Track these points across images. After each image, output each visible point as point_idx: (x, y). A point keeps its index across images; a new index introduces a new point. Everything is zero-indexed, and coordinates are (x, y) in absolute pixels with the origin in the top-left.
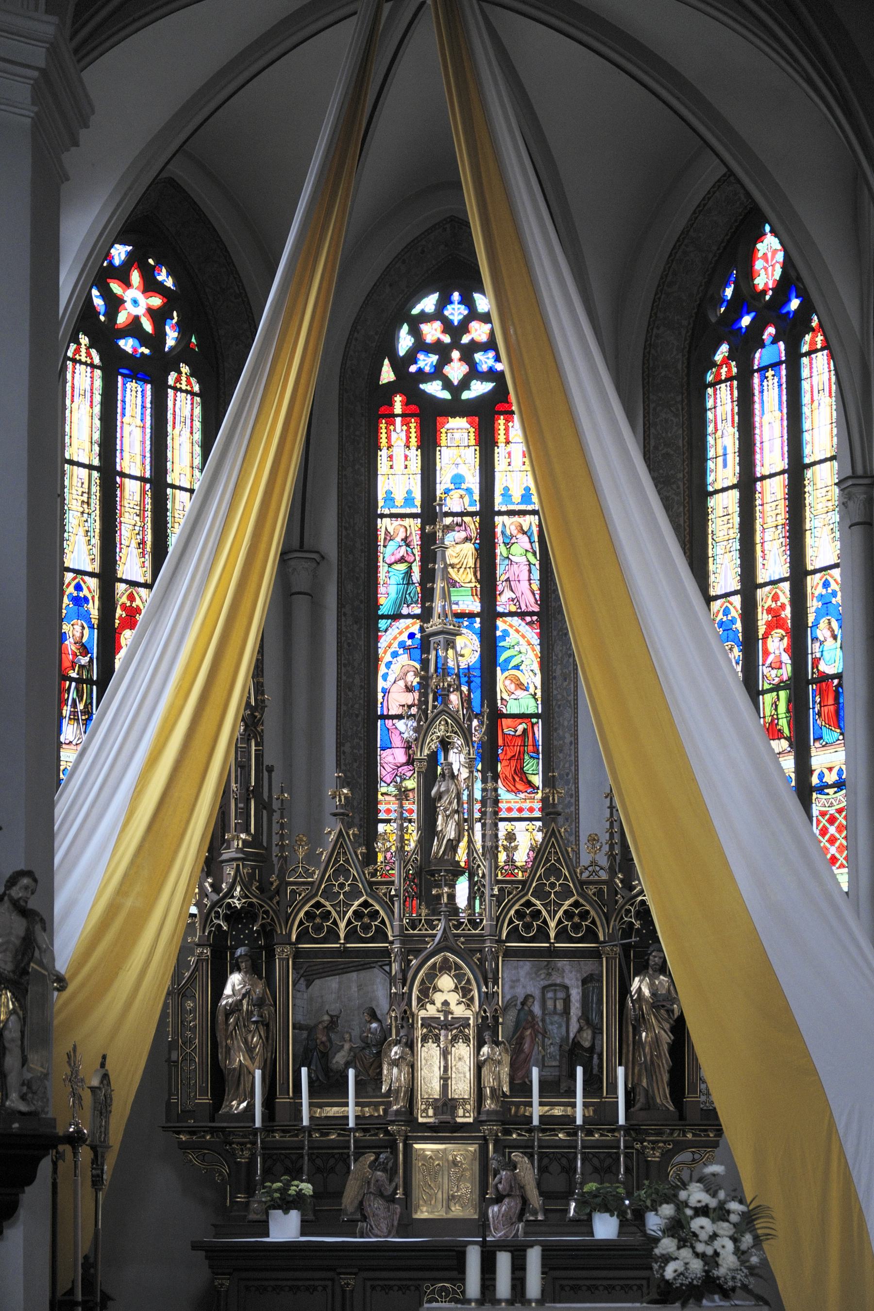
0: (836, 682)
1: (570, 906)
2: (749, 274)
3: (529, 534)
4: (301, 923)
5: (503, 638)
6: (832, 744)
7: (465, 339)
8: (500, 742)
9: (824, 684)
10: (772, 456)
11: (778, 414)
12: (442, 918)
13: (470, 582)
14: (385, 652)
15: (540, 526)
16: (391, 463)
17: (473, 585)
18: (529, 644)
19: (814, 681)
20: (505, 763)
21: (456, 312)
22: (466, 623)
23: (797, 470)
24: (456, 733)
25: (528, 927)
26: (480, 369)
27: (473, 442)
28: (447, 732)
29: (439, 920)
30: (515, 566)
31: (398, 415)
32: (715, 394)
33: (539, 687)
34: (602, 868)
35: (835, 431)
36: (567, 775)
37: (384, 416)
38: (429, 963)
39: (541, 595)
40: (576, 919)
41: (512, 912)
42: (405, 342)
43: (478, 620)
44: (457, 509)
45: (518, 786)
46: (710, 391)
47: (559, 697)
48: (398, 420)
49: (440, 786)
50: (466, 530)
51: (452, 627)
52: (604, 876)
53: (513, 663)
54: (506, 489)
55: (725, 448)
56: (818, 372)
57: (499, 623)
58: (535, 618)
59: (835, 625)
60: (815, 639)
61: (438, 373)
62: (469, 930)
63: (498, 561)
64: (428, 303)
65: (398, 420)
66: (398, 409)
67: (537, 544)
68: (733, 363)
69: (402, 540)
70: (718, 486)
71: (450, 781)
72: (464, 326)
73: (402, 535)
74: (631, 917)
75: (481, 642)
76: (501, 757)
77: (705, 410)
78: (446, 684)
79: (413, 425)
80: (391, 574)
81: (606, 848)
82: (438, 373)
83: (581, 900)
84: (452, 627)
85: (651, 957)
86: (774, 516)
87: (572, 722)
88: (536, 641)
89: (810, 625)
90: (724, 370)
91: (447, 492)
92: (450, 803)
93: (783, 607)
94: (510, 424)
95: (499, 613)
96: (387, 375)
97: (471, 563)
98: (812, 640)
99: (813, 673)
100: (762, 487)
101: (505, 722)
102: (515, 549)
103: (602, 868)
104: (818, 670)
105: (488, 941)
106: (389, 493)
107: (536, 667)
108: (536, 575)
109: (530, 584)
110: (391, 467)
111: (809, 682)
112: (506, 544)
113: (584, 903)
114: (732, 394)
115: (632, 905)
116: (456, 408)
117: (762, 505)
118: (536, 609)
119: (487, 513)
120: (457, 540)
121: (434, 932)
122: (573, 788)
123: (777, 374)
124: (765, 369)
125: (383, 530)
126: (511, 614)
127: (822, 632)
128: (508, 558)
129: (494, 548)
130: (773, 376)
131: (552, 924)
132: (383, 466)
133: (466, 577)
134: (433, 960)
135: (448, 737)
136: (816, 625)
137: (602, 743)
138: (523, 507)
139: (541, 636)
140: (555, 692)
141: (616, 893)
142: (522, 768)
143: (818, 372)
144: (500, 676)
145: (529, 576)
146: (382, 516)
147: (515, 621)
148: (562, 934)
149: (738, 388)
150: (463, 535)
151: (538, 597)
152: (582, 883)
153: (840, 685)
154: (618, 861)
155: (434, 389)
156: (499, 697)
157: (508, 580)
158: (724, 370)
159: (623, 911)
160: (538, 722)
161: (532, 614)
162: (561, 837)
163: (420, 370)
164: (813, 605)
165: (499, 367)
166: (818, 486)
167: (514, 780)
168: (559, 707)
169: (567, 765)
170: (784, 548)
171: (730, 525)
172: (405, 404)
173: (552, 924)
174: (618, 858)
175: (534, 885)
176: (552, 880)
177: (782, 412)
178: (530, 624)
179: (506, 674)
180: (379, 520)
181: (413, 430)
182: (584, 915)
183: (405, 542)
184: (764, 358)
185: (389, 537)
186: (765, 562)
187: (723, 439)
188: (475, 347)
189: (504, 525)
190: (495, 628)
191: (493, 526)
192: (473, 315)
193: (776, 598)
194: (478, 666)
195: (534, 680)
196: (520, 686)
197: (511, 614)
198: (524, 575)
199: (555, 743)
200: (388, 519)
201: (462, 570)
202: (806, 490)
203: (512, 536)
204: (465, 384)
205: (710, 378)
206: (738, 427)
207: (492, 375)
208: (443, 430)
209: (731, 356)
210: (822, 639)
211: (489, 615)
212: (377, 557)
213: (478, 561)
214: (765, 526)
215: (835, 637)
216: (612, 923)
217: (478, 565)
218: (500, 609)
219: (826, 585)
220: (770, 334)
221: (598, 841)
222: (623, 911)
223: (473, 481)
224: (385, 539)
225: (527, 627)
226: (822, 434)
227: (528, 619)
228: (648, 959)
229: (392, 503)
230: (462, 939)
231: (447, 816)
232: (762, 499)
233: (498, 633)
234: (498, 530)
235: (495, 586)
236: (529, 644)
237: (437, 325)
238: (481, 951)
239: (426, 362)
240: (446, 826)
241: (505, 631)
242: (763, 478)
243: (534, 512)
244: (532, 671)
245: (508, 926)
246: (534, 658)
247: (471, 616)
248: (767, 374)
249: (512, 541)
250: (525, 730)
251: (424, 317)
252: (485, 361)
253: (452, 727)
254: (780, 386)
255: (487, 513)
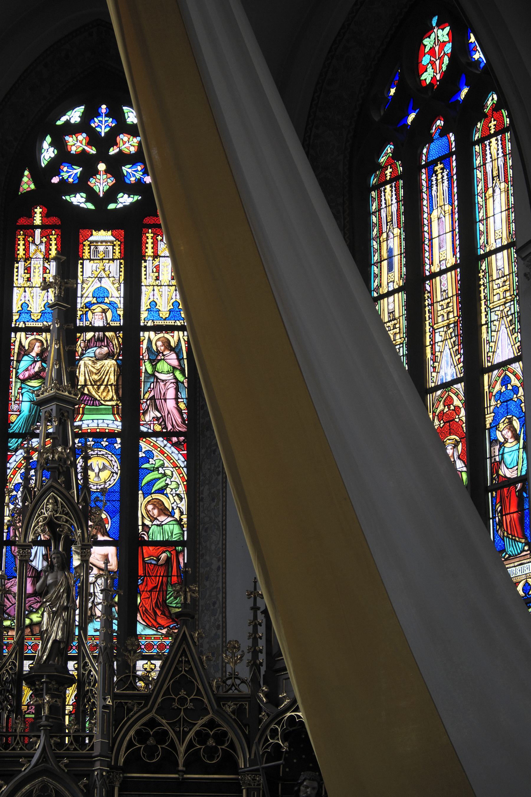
0: (519, 486)
1: (203, 725)
2: (417, 69)
3: (177, 351)
4: (130, 744)
5: (146, 460)
6: (515, 556)
7: (113, 151)
8: (141, 572)
9: (505, 490)
10: (442, 251)
11: (448, 208)
12: (42, 734)
13: (111, 400)
14: (14, 474)
15: (188, 342)
16: (28, 276)
17: (114, 403)
18: (175, 466)
19: (494, 488)
20: (145, 595)
21: (103, 125)
22: (105, 444)
23: (470, 261)
24: (67, 514)
25: (151, 751)
26: (127, 181)
27: (118, 255)
28: (56, 512)
29: (39, 737)
30: (162, 384)
31: (38, 227)
32: (380, 197)
33: (185, 512)
34: (243, 682)
35: (512, 216)
36: (214, 604)
37: (22, 228)
38: (24, 790)
39: (188, 414)
40: (211, 742)
41: (132, 733)
42: (48, 153)
43: (119, 440)
44: (99, 323)
45: (160, 620)
46: (374, 194)
47: (207, 519)
48: (38, 232)
49: (46, 577)
50: (107, 346)
51: (67, 394)
52: (245, 689)
53: (156, 487)
54: (154, 304)
55: (390, 251)
56: (494, 156)
57: (144, 445)
58: (182, 438)
59: (516, 424)
60: (494, 441)
61: (82, 185)
62: (75, 749)
63: (142, 378)
64: (75, 115)
65: (38, 232)
66: (38, 220)
67: (186, 361)
68: (399, 163)
69: (38, 355)
70: (384, 290)
71: (60, 573)
72: (111, 139)
73: (37, 349)
74: (278, 739)
75: (121, 464)
76: (141, 588)
77: (369, 214)
78: (56, 456)
79: (53, 237)
80: (24, 391)
81: (248, 656)
82: (82, 185)
83: (217, 719)
84: (67, 394)
85: (302, 788)
86: (445, 315)
87: (220, 545)
88: (182, 462)
89: (488, 426)
90: (388, 171)
91: (88, 306)
92: (59, 598)
93: (457, 409)
94: (159, 238)
95: (143, 432)
96: (27, 184)
97: (112, 379)
98: (491, 443)
99: (492, 479)
100: (431, 286)
101: (147, 550)
102: (162, 366)
103: (243, 682)
104: (498, 475)
105: (98, 763)
106: (24, 306)
107: (182, 490)
108: (184, 394)
109: (177, 403)
110: (29, 280)
111: (488, 490)
112: (151, 361)
113: (221, 722)
114: (397, 194)
115: (278, 723)
116: (101, 218)
117: (432, 305)
118: (183, 429)
119: (131, 326)
120: (98, 356)
121: (31, 751)
122: (220, 619)
123: (447, 166)
124: (434, 163)
125: (17, 344)
126: (156, 434)
127: (503, 433)
128: (153, 375)
129: (139, 365)
130: (442, 169)
131: (182, 749)
132: (19, 278)
133: (108, 396)
134: (27, 787)
135: (56, 518)
136: (495, 425)
137: (208, 391)
138: (171, 323)
139: (187, 458)
140: (202, 515)
141: (260, 710)
142: (165, 600)
143: (494, 156)
144: (142, 501)
145: (177, 395)
146: (17, 330)
147: (161, 441)
148: (194, 763)
149: (404, 187)
150: (105, 350)
151: (185, 416)
152: (219, 699)
153: (523, 489)
154: (263, 672)
155: (78, 199)
156: (140, 523)
157: (153, 398)
158: (388, 171)
159: (268, 732)
160: (183, 551)
161: (178, 434)
162: (194, 643)
163: (63, 181)
164: (491, 404)
165: (148, 180)
166: (495, 277)
167: (155, 614)
168: (206, 530)
169: (214, 593)
170: (457, 347)
171: (397, 330)
172: (44, 216)
173: (182, 749)
174: (263, 669)
175: (159, 700)
176: (183, 693)
177: (451, 204)
178: (175, 445)
179: (149, 498)
180: (13, 335)
181: (53, 242)
182: (221, 737)
183: (41, 357)
184: (432, 152)
185: (23, 352)
186: (436, 364)
187: (391, 242)
188: (124, 158)
189: (150, 341)
190: (138, 448)
191: (139, 342)
192: (121, 127)
193: (448, 402)
194: (117, 489)
195: (177, 501)
196: (164, 511)
197: (156, 434)
198: (171, 393)
199: (202, 570)
200: (23, 334)
201: (102, 387)
202: (481, 282)
203: (158, 352)
204: (111, 195)
205: (373, 181)
206: (404, 227)
207: (139, 187)
208: (86, 243)
209: (396, 155)
210: (502, 440)
211: (131, 434)
212: (9, 373)
213: (121, 378)
214: (435, 327)
215: (516, 437)
216: (254, 748)
217: (120, 383)
218: (143, 429)
219: (506, 381)
220: (438, 128)
221: (239, 648)
222: (268, 732)
223: (117, 295)
224: (19, 354)
225: (173, 449)
226: (496, 221)
227: (175, 439)
228: (299, 790)
229: (27, 316)
230: (66, 761)
231: (54, 613)
232: (432, 299)
233: (141, 455)
234: (144, 345)
235: (139, 404)
236: (175, 466)
237: (82, 137)
238: (89, 775)
239: (71, 173)
240: (52, 626)
241: (148, 452)
242: (434, 275)
243: (182, 328)
244: (178, 495)
245: (127, 749)
246: (179, 480)
247: (111, 435)
248: (436, 168)
249: (159, 358)
250: (168, 559)
251: (72, 129)
252: (132, 173)
253: (63, 506)
254: (450, 178)
255: (131, 326)
